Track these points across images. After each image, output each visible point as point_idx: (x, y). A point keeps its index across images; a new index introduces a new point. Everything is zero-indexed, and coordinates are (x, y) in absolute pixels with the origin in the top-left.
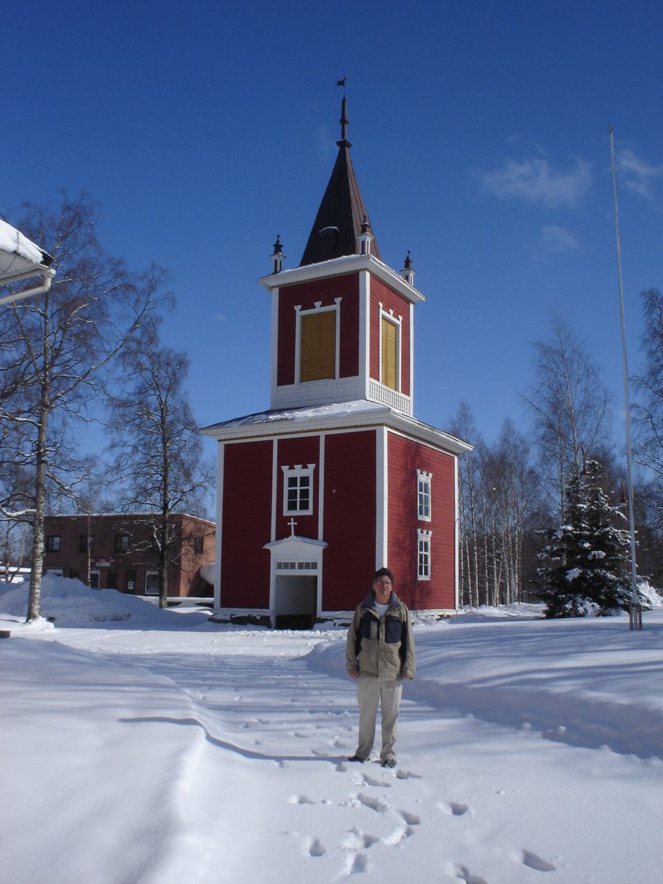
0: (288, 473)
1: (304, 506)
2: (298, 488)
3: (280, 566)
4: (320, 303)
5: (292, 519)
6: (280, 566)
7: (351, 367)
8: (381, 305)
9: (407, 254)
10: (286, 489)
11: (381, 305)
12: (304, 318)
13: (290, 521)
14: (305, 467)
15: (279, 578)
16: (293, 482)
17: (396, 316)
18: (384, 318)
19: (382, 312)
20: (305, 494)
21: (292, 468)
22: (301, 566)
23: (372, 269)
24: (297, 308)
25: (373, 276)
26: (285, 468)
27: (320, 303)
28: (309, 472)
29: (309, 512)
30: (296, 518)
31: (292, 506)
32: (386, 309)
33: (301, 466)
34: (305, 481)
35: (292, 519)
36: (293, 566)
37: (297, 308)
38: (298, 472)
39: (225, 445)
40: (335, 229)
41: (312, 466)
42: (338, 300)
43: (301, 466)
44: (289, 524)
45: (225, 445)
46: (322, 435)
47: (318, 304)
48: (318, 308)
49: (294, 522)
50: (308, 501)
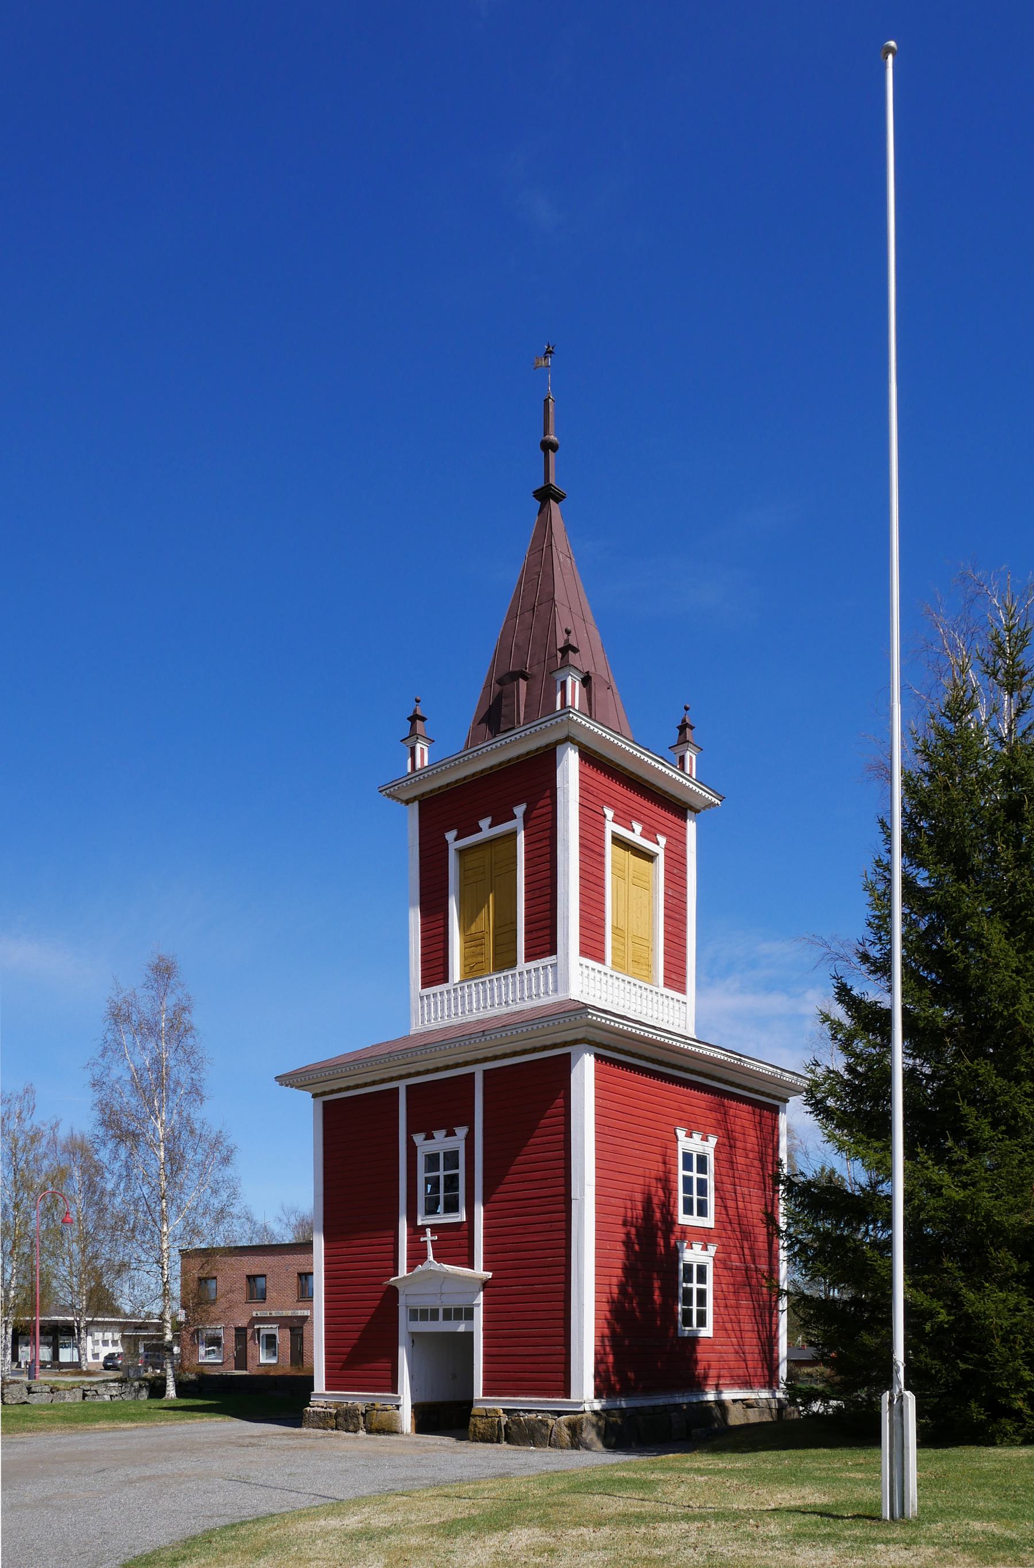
0: (424, 1147)
1: (452, 1207)
2: (442, 1173)
3: (416, 1315)
4: (488, 821)
5: (428, 1230)
6: (416, 1315)
7: (544, 941)
8: (609, 813)
9: (566, 636)
10: (422, 1175)
11: (609, 813)
12: (461, 852)
13: (425, 1234)
14: (451, 1133)
15: (416, 1338)
16: (432, 1161)
17: (649, 833)
18: (617, 840)
19: (611, 827)
20: (452, 1182)
21: (430, 1137)
22: (448, 1315)
23: (582, 739)
24: (450, 836)
25: (588, 756)
26: (419, 1138)
27: (488, 821)
28: (457, 1142)
29: (461, 1216)
30: (435, 1228)
31: (431, 1211)
32: (624, 818)
33: (444, 1132)
34: (452, 1159)
35: (428, 1230)
36: (434, 1315)
37: (450, 836)
38: (441, 1143)
39: (324, 1103)
40: (520, 678)
41: (462, 1132)
42: (519, 810)
43: (444, 1132)
44: (422, 1239)
45: (324, 1103)
46: (478, 1071)
47: (485, 823)
48: (487, 830)
49: (432, 1234)
50: (458, 1195)
